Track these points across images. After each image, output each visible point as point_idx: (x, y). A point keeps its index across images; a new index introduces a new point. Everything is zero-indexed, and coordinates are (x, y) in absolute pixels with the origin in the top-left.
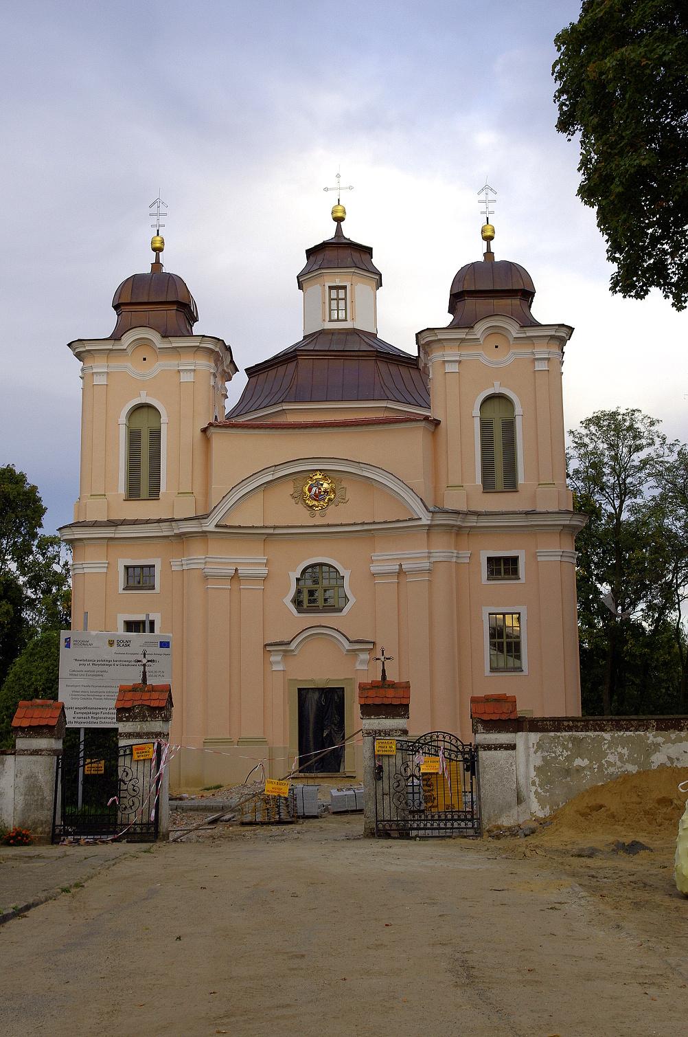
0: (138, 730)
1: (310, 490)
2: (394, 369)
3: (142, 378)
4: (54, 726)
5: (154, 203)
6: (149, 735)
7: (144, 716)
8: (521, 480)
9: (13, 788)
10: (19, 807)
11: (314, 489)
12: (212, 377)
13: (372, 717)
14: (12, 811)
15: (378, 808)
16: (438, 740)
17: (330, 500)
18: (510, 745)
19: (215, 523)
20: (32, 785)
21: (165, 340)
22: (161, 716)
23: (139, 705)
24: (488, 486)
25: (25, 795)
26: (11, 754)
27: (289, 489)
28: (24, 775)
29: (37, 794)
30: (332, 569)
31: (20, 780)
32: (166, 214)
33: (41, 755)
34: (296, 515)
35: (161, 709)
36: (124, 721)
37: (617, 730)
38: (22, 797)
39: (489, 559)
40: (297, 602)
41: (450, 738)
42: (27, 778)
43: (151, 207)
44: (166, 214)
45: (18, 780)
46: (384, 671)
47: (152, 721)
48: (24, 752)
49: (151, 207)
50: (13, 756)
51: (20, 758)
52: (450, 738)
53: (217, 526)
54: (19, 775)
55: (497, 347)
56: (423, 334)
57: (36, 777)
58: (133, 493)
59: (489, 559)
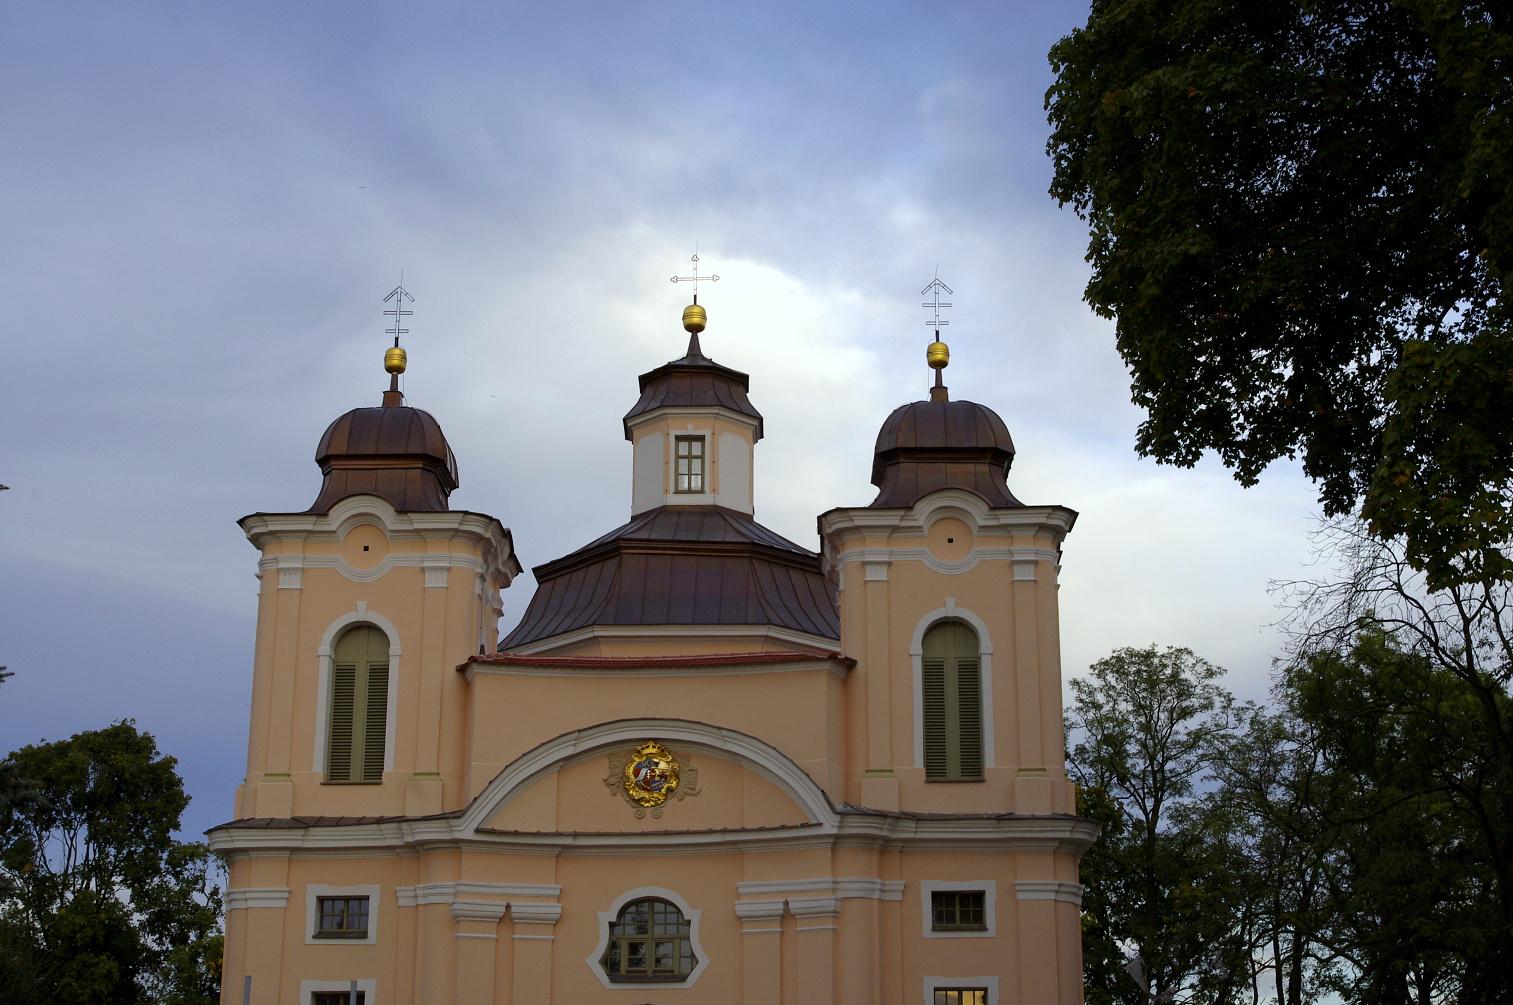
1: (637, 773)
2: (780, 574)
5: (392, 295)
8: (989, 762)
11: (643, 772)
12: (478, 581)
17: (670, 790)
21: (403, 517)
24: (935, 770)
27: (601, 769)
34: (617, 815)
39: (937, 897)
40: (610, 964)
43: (386, 300)
49: (386, 300)
53: (478, 831)
55: (950, 541)
56: (830, 517)
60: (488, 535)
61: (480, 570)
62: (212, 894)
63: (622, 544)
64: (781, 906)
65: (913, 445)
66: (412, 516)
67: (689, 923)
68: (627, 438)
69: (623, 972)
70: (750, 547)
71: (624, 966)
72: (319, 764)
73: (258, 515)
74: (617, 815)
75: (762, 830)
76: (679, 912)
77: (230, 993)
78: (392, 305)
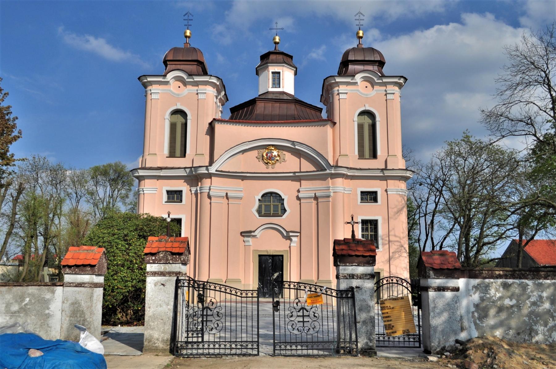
0: (162, 270)
1: (267, 155)
2: (303, 108)
3: (177, 96)
4: (95, 266)
5: (186, 14)
6: (170, 274)
7: (167, 260)
8: (379, 153)
9: (61, 311)
10: (65, 326)
11: (269, 155)
12: (215, 98)
13: (348, 264)
14: (59, 329)
15: (343, 332)
16: (392, 283)
17: (277, 160)
18: (455, 288)
19: (215, 169)
20: (76, 309)
21: (191, 77)
22: (181, 260)
23: (163, 251)
24: (361, 156)
25: (70, 317)
26: (60, 286)
27: (255, 153)
28: (70, 302)
29: (80, 316)
30: (277, 195)
31: (67, 305)
32: (192, 20)
33: (83, 287)
34: (261, 167)
35: (180, 254)
36: (151, 263)
37: (537, 279)
38: (68, 319)
39: (362, 192)
40: (259, 211)
41: (402, 281)
42: (73, 304)
43: (184, 16)
44: (192, 20)
45: (64, 305)
46: (353, 231)
47: (173, 263)
48: (70, 285)
49: (184, 16)
50: (61, 287)
51: (67, 289)
52: (402, 281)
53: (216, 171)
54: (65, 302)
55: (366, 87)
56: (328, 79)
57: (79, 303)
58: (172, 154)
59: (362, 192)
60: (218, 84)
61: (215, 94)
62: (350, 277)
63: (257, 99)
64: (314, 194)
65: (354, 59)
66: (194, 77)
67: (283, 200)
68: (256, 74)
69: (263, 213)
70: (295, 101)
71: (263, 212)
72: (166, 151)
73: (144, 76)
74: (261, 167)
75: (307, 172)
76: (280, 196)
77: (554, 263)
78: (186, 17)
